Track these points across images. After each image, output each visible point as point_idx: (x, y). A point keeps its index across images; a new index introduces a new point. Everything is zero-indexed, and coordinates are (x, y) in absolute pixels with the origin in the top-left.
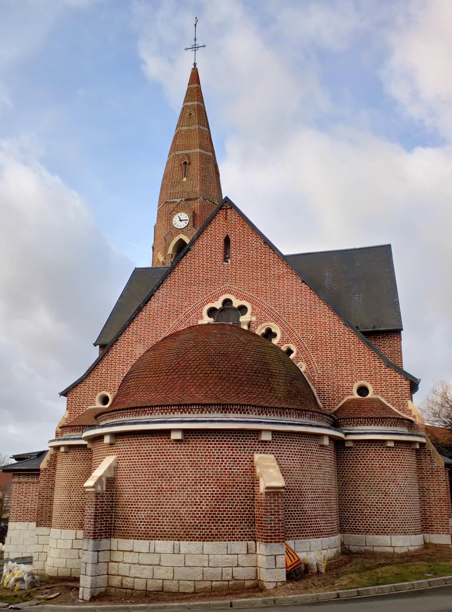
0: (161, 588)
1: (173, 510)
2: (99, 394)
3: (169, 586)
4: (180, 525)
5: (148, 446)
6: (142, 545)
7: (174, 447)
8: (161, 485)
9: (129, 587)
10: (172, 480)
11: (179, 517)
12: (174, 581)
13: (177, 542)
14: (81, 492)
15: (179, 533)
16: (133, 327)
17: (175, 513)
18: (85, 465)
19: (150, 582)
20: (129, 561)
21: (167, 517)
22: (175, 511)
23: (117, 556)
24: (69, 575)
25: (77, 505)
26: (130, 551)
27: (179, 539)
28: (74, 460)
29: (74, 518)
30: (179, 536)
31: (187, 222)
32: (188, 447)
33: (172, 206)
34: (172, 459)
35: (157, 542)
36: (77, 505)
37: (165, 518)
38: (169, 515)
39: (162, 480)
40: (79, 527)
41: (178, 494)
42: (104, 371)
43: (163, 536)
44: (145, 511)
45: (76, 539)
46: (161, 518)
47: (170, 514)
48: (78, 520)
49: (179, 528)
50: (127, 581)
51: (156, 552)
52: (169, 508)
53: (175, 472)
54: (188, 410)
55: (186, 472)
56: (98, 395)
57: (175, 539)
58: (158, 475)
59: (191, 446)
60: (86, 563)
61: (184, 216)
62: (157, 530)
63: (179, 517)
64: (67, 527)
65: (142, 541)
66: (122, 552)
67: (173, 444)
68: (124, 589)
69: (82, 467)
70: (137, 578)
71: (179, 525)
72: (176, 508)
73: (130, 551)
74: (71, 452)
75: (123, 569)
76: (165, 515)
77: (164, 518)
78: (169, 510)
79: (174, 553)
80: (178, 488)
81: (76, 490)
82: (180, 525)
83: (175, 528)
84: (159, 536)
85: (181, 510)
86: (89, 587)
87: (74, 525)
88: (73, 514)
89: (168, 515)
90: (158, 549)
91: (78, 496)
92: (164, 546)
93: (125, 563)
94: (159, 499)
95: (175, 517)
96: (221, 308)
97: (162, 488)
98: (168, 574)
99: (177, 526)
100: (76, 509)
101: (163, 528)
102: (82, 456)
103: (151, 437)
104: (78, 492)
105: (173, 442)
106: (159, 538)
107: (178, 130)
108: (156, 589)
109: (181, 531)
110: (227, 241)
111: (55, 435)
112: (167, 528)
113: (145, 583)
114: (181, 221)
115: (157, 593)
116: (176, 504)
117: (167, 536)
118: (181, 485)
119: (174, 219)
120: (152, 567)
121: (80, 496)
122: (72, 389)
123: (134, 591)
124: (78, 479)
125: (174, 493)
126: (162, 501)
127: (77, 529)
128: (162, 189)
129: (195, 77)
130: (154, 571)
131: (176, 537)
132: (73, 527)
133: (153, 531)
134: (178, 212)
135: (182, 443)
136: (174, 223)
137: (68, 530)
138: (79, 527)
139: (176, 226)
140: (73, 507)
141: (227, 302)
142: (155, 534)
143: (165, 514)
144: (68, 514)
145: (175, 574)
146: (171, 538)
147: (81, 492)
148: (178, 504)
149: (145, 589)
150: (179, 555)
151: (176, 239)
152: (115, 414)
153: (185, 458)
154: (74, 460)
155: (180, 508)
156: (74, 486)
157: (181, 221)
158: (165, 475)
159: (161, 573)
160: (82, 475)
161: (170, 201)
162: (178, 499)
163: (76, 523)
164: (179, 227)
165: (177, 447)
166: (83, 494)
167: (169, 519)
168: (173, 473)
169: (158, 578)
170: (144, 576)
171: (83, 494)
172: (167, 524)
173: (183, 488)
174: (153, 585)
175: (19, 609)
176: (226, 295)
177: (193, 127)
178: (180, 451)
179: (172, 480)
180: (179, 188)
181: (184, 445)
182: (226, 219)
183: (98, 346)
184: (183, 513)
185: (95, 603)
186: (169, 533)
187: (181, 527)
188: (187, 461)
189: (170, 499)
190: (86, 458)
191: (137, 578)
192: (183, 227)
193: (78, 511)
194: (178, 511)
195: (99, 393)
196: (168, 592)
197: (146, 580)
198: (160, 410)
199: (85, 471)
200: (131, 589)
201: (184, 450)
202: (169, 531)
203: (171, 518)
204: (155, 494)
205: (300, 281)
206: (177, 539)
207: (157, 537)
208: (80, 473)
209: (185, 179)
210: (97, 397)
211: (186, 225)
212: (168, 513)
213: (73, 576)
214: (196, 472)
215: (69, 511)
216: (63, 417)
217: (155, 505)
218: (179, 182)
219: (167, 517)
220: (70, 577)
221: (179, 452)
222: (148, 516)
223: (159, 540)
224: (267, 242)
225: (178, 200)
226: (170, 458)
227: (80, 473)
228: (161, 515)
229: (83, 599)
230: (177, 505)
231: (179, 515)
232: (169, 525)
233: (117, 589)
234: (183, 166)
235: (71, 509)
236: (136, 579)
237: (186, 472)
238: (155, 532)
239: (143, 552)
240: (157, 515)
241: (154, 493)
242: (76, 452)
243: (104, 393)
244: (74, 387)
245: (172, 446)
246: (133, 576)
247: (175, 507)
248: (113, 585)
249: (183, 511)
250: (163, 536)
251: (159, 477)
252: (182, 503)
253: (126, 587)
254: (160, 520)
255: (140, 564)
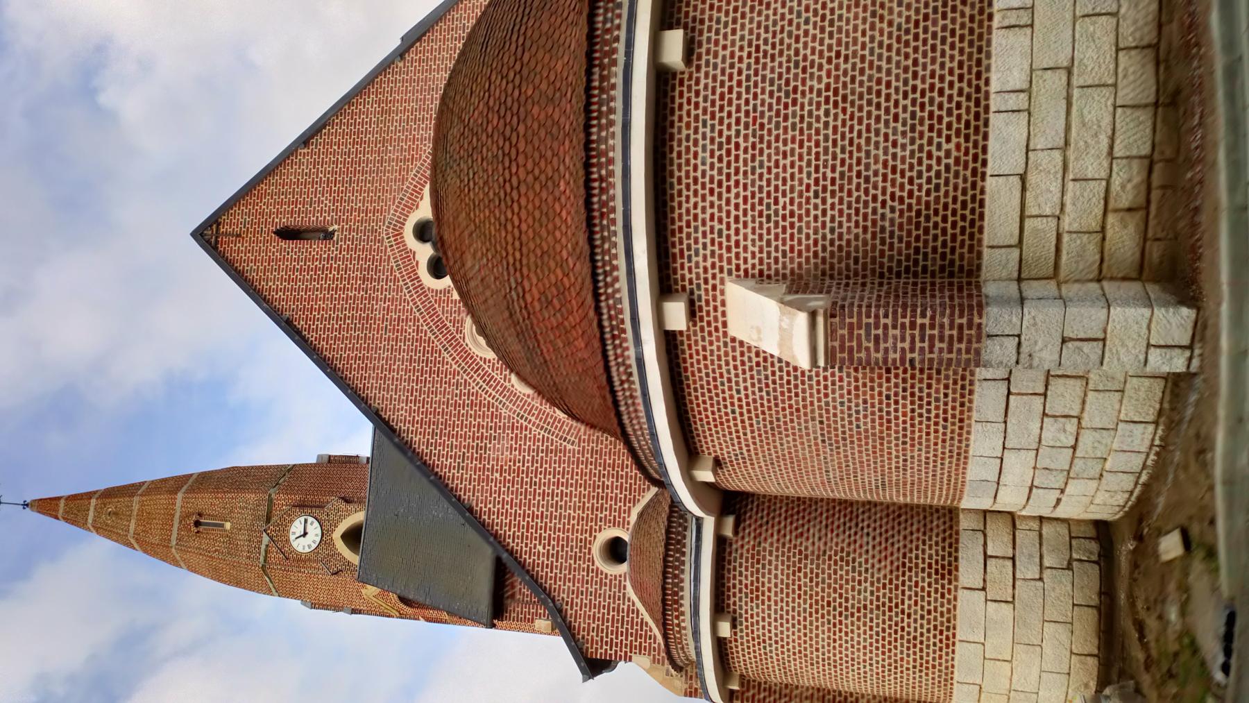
0: (1146, 51)
1: (895, 46)
2: (600, 563)
3: (1141, 23)
4: (944, 16)
5: (698, 155)
6: (1005, 141)
7: (707, 64)
8: (819, 94)
9: (1145, 174)
10: (805, 59)
11: (917, 24)
12: (1123, 11)
13: (996, 23)
14: (847, 572)
15: (967, 20)
16: (445, 464)
17: (904, 38)
18: (773, 558)
19: (1127, 94)
20: (1055, 187)
21: (915, 63)
22: (899, 40)
23: (1041, 231)
24: (1095, 612)
25: (884, 587)
26: (1024, 189)
27: (985, 16)
28: (756, 593)
29: (923, 598)
30: (977, 18)
31: (310, 519)
32: (711, 19)
33: (275, 555)
34: (744, 66)
35: (994, 86)
36: (884, 587)
37: (919, 69)
38: (912, 56)
39: (803, 93)
40: (950, 583)
41: (847, 36)
42: (541, 548)
43: (975, 70)
44: (895, 144)
45: (984, 589)
46: (918, 82)
47: (907, 56)
48: (930, 585)
49: (953, 21)
50: (1123, 187)
51: (1025, 86)
52: (889, 60)
53: (781, 53)
54: (606, 43)
55: (783, 18)
56: (601, 568)
57: (985, 30)
58: (786, 107)
59: (708, 12)
60: (1064, 341)
61: (297, 527)
62: (955, 92)
63: (917, 24)
64: (948, 621)
65: (992, 144)
66: (1029, 224)
67: (698, 68)
68: (1148, 201)
69: (776, 569)
70: (1111, 147)
71: (941, 23)
72: (890, 37)
73: (1024, 189)
74: (735, 604)
75: (1083, 209)
76: (912, 69)
77: (921, 73)
78: (895, 58)
79: (1032, 26)
80: (831, 37)
81: (841, 588)
82: (944, 16)
83: (953, 33)
84: (974, 82)
85: (897, 20)
86: (1147, 312)
87: (943, 596)
88: (910, 598)
89: (910, 62)
90: (1017, 79)
91: (860, 583)
92: (1007, 64)
93: (1063, 205)
94: (861, 97)
95: (916, 38)
96: (435, 246)
97: (828, 88)
98: (1098, 34)
99: (944, 28)
100: (897, 589)
101: (951, 72)
102: (747, 570)
103: (675, 144)
104: (847, 581)
105: (694, 69)
106: (982, 83)
107: (133, 541)
108: (1150, 68)
109: (963, 15)
110: (288, 234)
111: (693, 699)
112: (952, 58)
113: (1129, 111)
114: (305, 534)
115: (1162, 68)
116: (878, 38)
117: (975, 56)
118: (822, 30)
119: (300, 549)
120: (1076, 93)
121: (860, 575)
122: (576, 641)
123: (1156, 156)
124: (811, 581)
125: (843, 48)
126: (866, 84)
127: (956, 588)
128: (238, 584)
129: (46, 506)
130: (1089, 82)
131: (980, 26)
132: (949, 601)
133: (959, 106)
134: (288, 541)
135: (697, 39)
136: (307, 550)
137: (958, 617)
138: (950, 583)
139: (314, 546)
140: (890, 600)
141: (422, 232)
142: (969, 98)
143: (906, 70)
144: (909, 616)
145: (1098, 10)
146: (984, 43)
147: (847, 573)
148: (877, 34)
149: (1150, 111)
150: (1038, 9)
151: (341, 547)
152: (637, 437)
153: (743, 26)
154: (756, 593)
155: (890, 24)
156: (829, 595)
157: (305, 534)
158: (787, 83)
159: (1095, 56)
160: (800, 570)
161: (262, 559)
162: (864, 34)
163: (936, 591)
164: (318, 539)
165: (708, 53)
166: (854, 568)
167: (925, 55)
168: (784, 59)
169: (1112, 66)
170: (1107, 120)
171: (854, 568)
172: (939, 60)
173: (832, 24)
174: (1137, 81)
175: (1231, 620)
176: (405, 235)
177: (136, 507)
178: (722, 42)
179: (805, 59)
180: (242, 537)
181: (706, 35)
182: (238, 236)
183: (495, 621)
184: (905, 13)
185: (1206, 288)
186: (967, 50)
187: (950, 15)
188: (751, 21)
189: (863, 58)
190: (753, 558)
191: (1111, 147)
192: (319, 531)
193: (903, 584)
194: (899, 29)
195: (597, 563)
196: (1160, 26)
197: (1119, 111)
198: (600, 127)
199: (789, 558)
200: (1150, 171)
201: (717, 33)
202: (961, 51)
203: (921, 49)
204: (844, 110)
205: (401, 64)
206: (986, 23)
207: (978, 89)
208: (794, 574)
209: (228, 525)
210: (605, 571)
211: (316, 524)
212: (903, 63)
213: (1095, 600)
214: (846, 634)
215: (903, 612)
216: (648, 671)
217: (878, 106)
218: (230, 537)
219: (915, 63)
220: (1098, 608)
221: (724, 47)
222: (913, 129)
223: (987, 82)
224: (305, 140)
225: (266, 539)
226: (740, 73)
227: (794, 574)
228: (911, 82)
229: (1190, 347)
230: (882, 34)
231: (912, 25)
232: (943, 54)
233: (1150, 234)
234: (201, 528)
235: (897, 606)
236: (1118, 151)
237: (783, 18)
238: (963, 99)
239: (1025, 134)
240: (911, 96)
241: (841, 116)
242: (734, 587)
243: (596, 549)
244: (573, 636)
245: (703, 69)
246: (1106, 164)
247: (886, 42)
248: (1138, 255)
249: (900, 14)
250: (975, 70)
251: (794, 102)
252: (877, 20)
253: (1143, 188)
254: (927, 86)
255: (1067, 143)
